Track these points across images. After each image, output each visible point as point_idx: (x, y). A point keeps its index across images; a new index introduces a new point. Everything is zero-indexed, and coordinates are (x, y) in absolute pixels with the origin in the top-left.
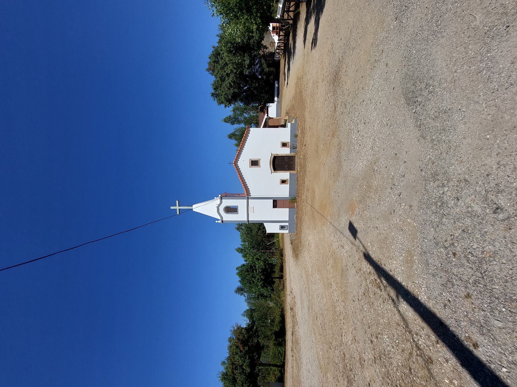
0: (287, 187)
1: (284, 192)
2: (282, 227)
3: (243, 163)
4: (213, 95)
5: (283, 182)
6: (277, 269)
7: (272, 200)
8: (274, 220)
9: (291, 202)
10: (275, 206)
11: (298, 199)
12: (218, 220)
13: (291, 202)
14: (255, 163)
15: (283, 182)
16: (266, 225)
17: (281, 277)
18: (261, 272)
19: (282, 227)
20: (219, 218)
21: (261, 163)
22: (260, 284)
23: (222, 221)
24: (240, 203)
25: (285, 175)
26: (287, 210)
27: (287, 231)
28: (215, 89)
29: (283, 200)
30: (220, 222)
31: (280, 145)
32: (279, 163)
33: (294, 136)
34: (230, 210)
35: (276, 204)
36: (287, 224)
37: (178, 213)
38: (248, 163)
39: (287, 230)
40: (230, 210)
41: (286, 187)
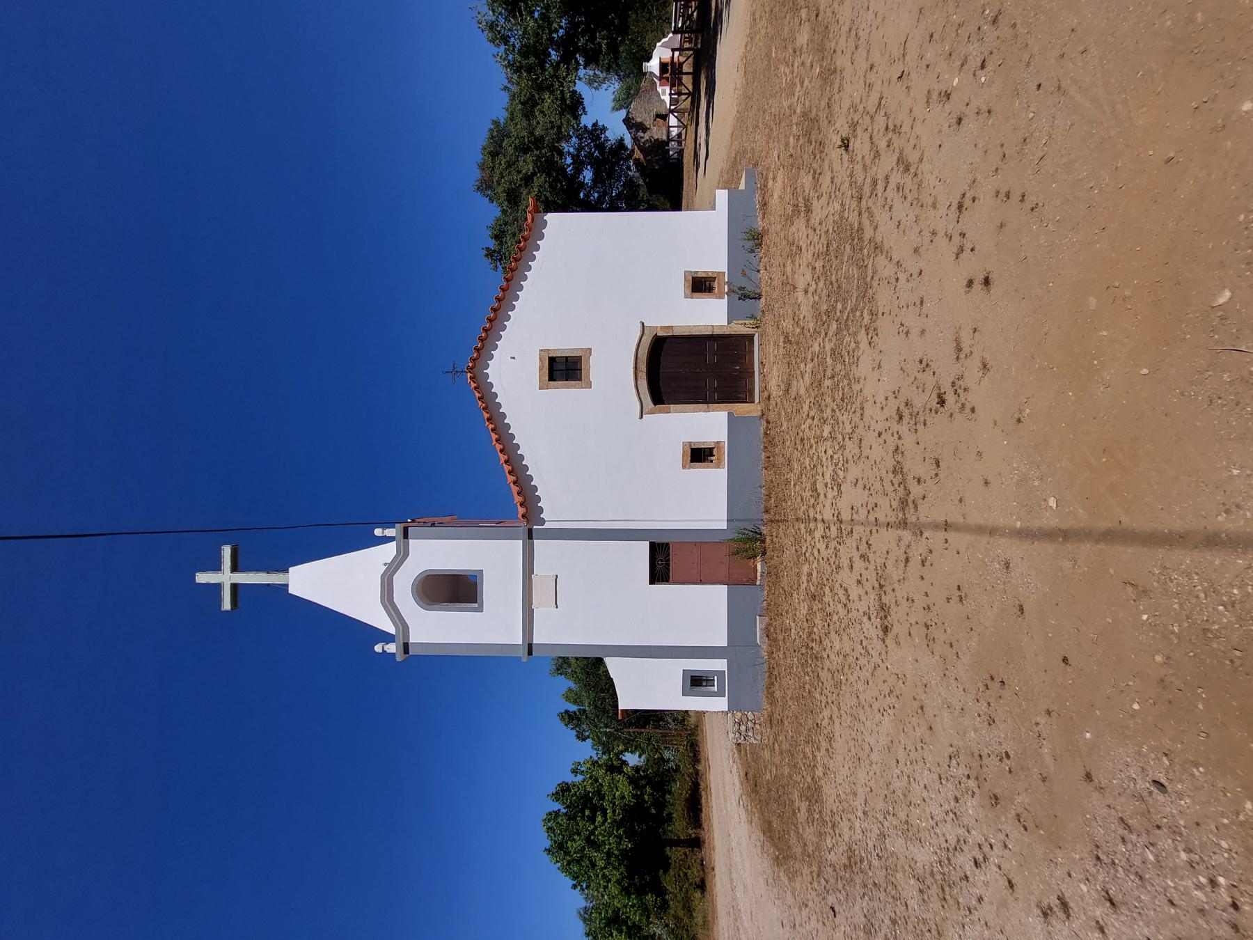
0: (715, 478)
1: (704, 504)
2: (696, 682)
3: (512, 371)
4: (490, 253)
5: (699, 455)
6: (677, 809)
7: (644, 547)
8: (664, 645)
9: (737, 556)
10: (659, 573)
11: (781, 538)
12: (388, 638)
13: (737, 556)
14: (564, 369)
15: (699, 455)
16: (614, 666)
17: (696, 843)
18: (618, 824)
19: (696, 682)
20: (391, 629)
21: (596, 369)
22: (615, 875)
23: (406, 647)
24: (490, 557)
25: (709, 423)
26: (718, 595)
27: (721, 704)
28: (496, 237)
29: (699, 542)
30: (391, 648)
31: (680, 286)
32: (680, 369)
33: (748, 239)
34: (456, 590)
35: (664, 562)
36: (720, 665)
37: (227, 605)
38: (534, 369)
39: (720, 694)
40: (456, 590)
41: (713, 482)
